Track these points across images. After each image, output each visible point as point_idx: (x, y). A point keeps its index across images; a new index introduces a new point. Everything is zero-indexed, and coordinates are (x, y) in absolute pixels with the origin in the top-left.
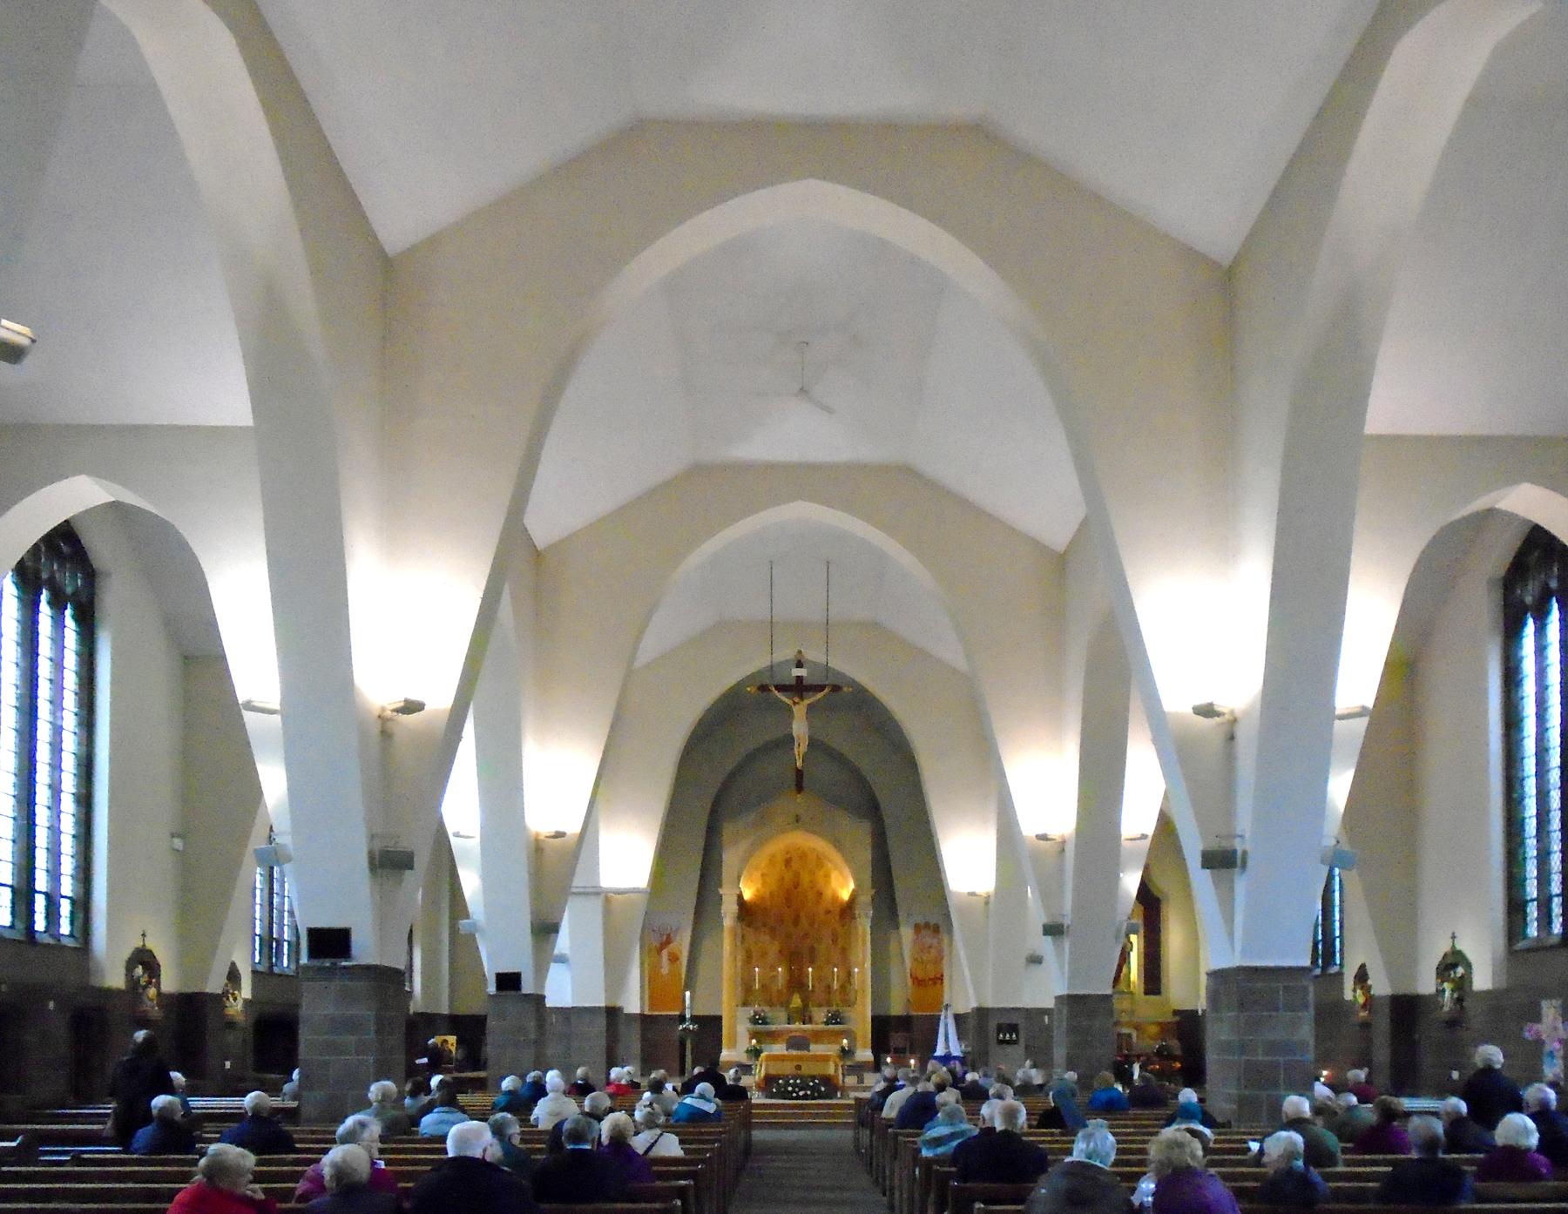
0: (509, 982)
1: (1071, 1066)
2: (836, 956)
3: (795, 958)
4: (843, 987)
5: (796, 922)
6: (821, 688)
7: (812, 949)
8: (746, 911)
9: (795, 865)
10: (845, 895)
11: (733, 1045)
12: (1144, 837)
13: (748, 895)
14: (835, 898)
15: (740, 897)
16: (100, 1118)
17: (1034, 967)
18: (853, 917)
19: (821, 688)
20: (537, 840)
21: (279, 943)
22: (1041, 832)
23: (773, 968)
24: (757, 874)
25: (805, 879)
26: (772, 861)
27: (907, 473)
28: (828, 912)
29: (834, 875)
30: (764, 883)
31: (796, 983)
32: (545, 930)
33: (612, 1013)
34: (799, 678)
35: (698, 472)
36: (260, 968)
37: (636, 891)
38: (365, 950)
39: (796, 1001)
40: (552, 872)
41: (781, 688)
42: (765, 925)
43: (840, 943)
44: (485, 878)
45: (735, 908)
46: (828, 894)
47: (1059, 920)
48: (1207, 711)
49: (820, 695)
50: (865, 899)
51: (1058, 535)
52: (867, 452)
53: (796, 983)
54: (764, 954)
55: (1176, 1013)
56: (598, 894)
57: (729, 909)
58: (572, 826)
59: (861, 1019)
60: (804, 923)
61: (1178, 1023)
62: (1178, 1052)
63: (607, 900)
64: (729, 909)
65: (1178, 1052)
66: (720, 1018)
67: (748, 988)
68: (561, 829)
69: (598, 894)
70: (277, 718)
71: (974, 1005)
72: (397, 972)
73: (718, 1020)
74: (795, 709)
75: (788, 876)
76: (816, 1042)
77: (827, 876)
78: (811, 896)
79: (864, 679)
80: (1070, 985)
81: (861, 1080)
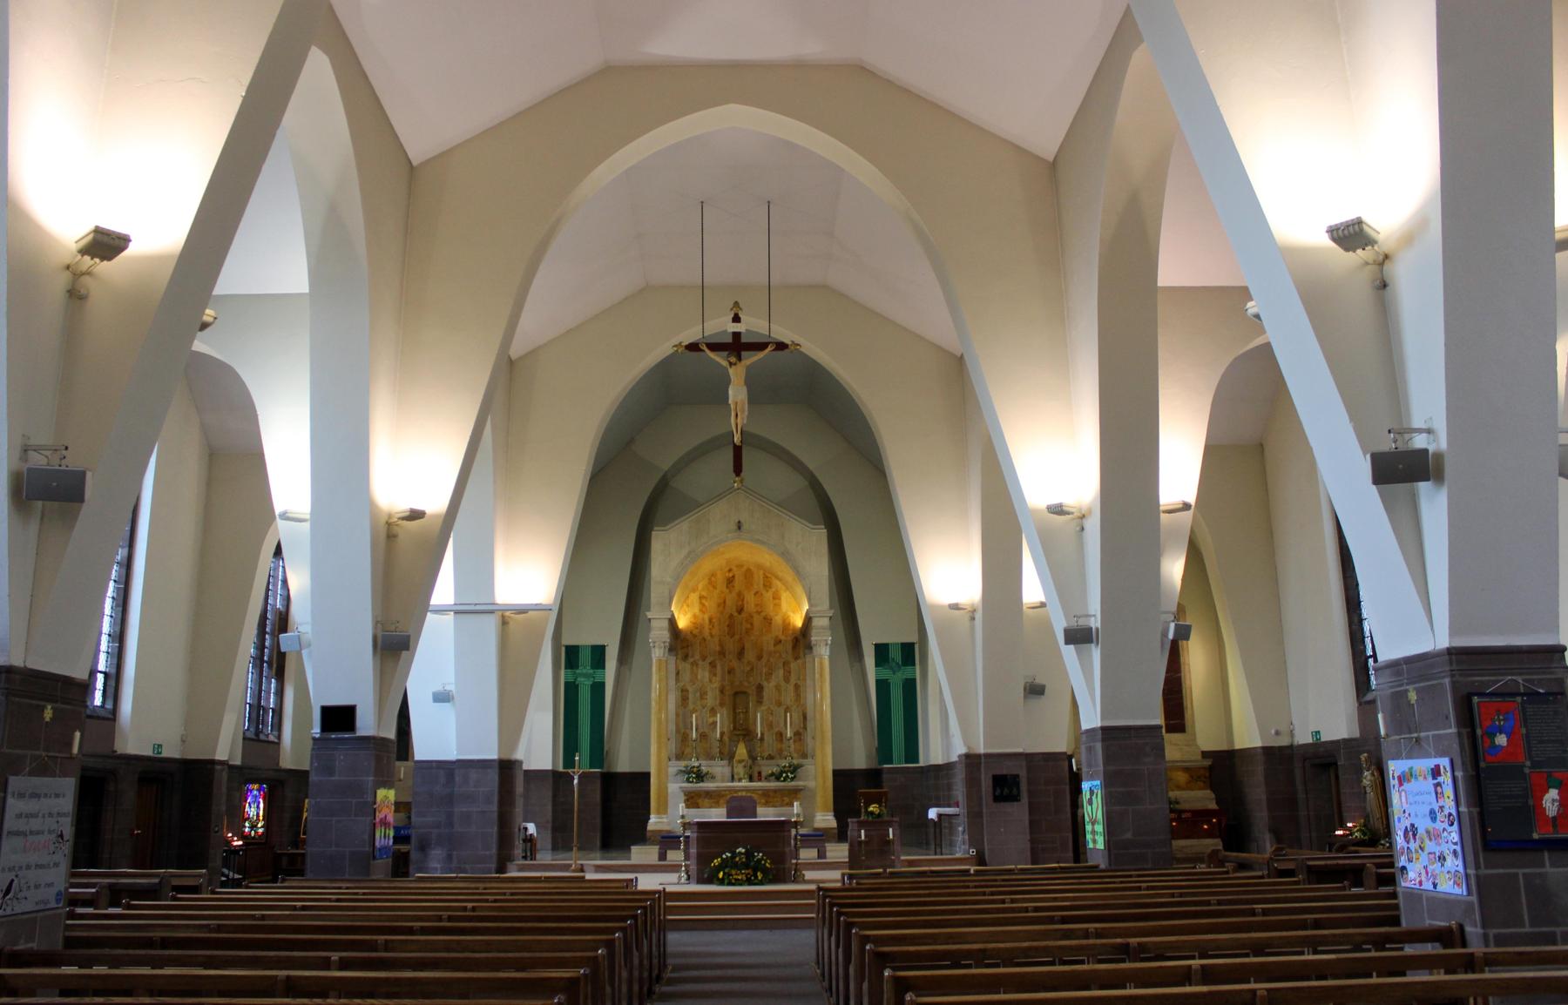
0: (339, 718)
1: (940, 816)
2: (789, 697)
3: (738, 699)
4: (798, 735)
5: (741, 653)
6: (760, 346)
7: (760, 688)
8: (679, 642)
9: (738, 585)
10: (798, 622)
11: (663, 809)
12: (1186, 506)
13: (683, 622)
14: (786, 625)
15: (672, 622)
16: (200, 876)
17: (1036, 702)
18: (809, 647)
19: (760, 346)
20: (389, 524)
21: (266, 710)
22: (1054, 501)
23: (713, 711)
24: (694, 597)
25: (750, 599)
26: (712, 583)
27: (861, 71)
28: (778, 642)
29: (785, 597)
30: (703, 609)
31: (742, 731)
32: (393, 647)
33: (506, 767)
34: (737, 335)
35: (608, 72)
36: (249, 735)
37: (538, 608)
38: (367, 724)
39: (742, 751)
40: (401, 560)
41: (714, 347)
42: (704, 658)
43: (793, 680)
44: (316, 577)
45: (666, 635)
46: (778, 620)
47: (1082, 622)
48: (1351, 235)
49: (761, 355)
50: (821, 622)
51: (1046, 139)
52: (812, 48)
53: (742, 731)
54: (703, 695)
55: (1205, 754)
56: (492, 612)
57: (658, 634)
58: (435, 502)
59: (818, 777)
60: (750, 655)
61: (1211, 768)
62: (1213, 806)
63: (504, 622)
64: (658, 634)
65: (1213, 806)
66: (647, 775)
67: (684, 738)
68: (418, 507)
69: (492, 612)
70: (307, 526)
71: (962, 750)
72: (67, 681)
73: (645, 777)
74: (731, 371)
75: (731, 600)
76: (767, 804)
77: (776, 597)
78: (757, 620)
79: (813, 349)
80: (1102, 719)
81: (822, 855)
